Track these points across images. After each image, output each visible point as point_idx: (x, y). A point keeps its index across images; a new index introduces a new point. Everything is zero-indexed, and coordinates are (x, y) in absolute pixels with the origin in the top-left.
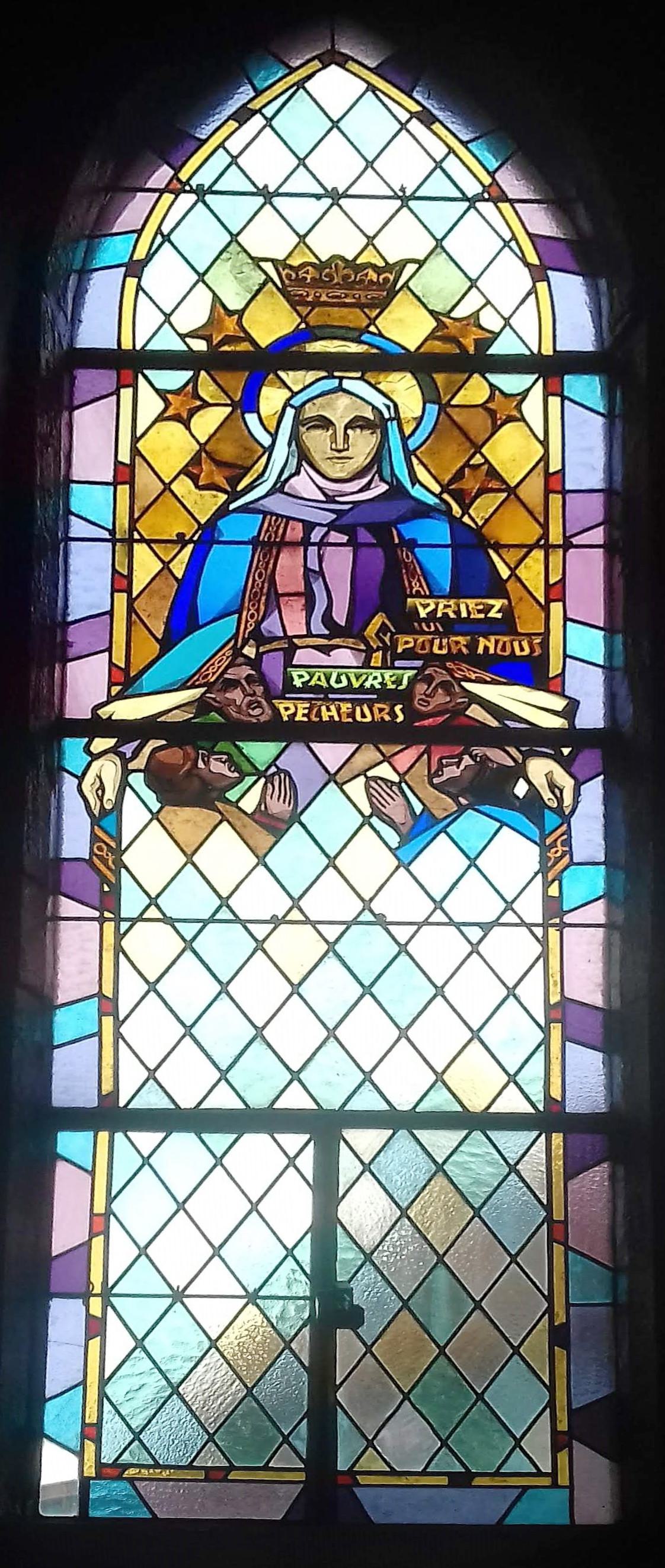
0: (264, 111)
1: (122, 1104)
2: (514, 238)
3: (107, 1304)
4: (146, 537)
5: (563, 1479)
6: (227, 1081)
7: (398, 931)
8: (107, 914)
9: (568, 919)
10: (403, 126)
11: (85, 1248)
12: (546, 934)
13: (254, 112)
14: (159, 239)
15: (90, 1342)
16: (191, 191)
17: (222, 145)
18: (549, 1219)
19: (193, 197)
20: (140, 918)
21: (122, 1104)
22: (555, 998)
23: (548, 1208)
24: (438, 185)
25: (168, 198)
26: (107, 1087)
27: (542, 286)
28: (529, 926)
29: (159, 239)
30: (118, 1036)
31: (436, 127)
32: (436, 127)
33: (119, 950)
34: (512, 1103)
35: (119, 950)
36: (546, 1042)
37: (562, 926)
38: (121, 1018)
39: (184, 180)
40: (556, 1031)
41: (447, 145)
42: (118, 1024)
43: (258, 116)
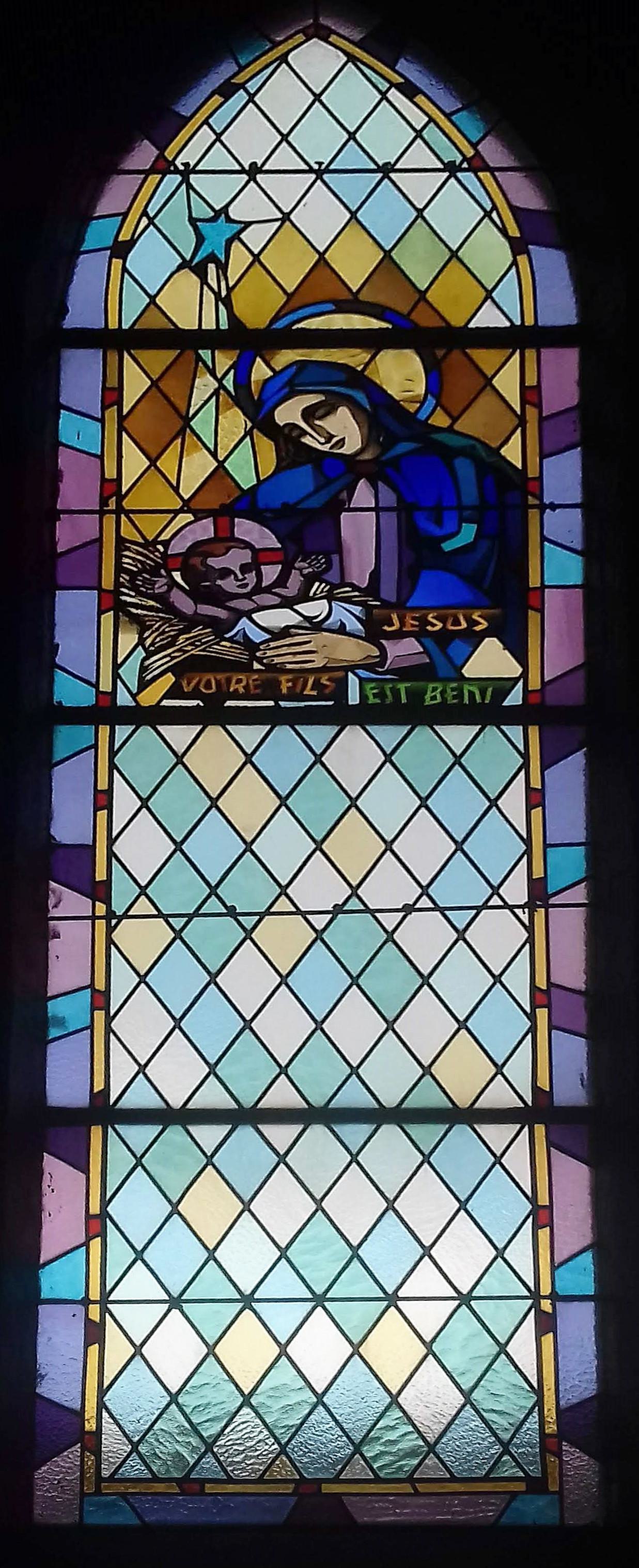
2: (495, 207)
3: (105, 1311)
5: (553, 1487)
7: (525, 918)
9: (552, 901)
14: (144, 221)
16: (177, 171)
17: (206, 122)
19: (179, 178)
22: (542, 983)
25: (154, 178)
26: (99, 1086)
27: (522, 260)
29: (144, 221)
30: (109, 1030)
31: (420, 99)
32: (420, 99)
33: (110, 942)
35: (110, 942)
36: (533, 1030)
37: (547, 907)
40: (542, 1014)
42: (109, 1019)
43: (242, 91)
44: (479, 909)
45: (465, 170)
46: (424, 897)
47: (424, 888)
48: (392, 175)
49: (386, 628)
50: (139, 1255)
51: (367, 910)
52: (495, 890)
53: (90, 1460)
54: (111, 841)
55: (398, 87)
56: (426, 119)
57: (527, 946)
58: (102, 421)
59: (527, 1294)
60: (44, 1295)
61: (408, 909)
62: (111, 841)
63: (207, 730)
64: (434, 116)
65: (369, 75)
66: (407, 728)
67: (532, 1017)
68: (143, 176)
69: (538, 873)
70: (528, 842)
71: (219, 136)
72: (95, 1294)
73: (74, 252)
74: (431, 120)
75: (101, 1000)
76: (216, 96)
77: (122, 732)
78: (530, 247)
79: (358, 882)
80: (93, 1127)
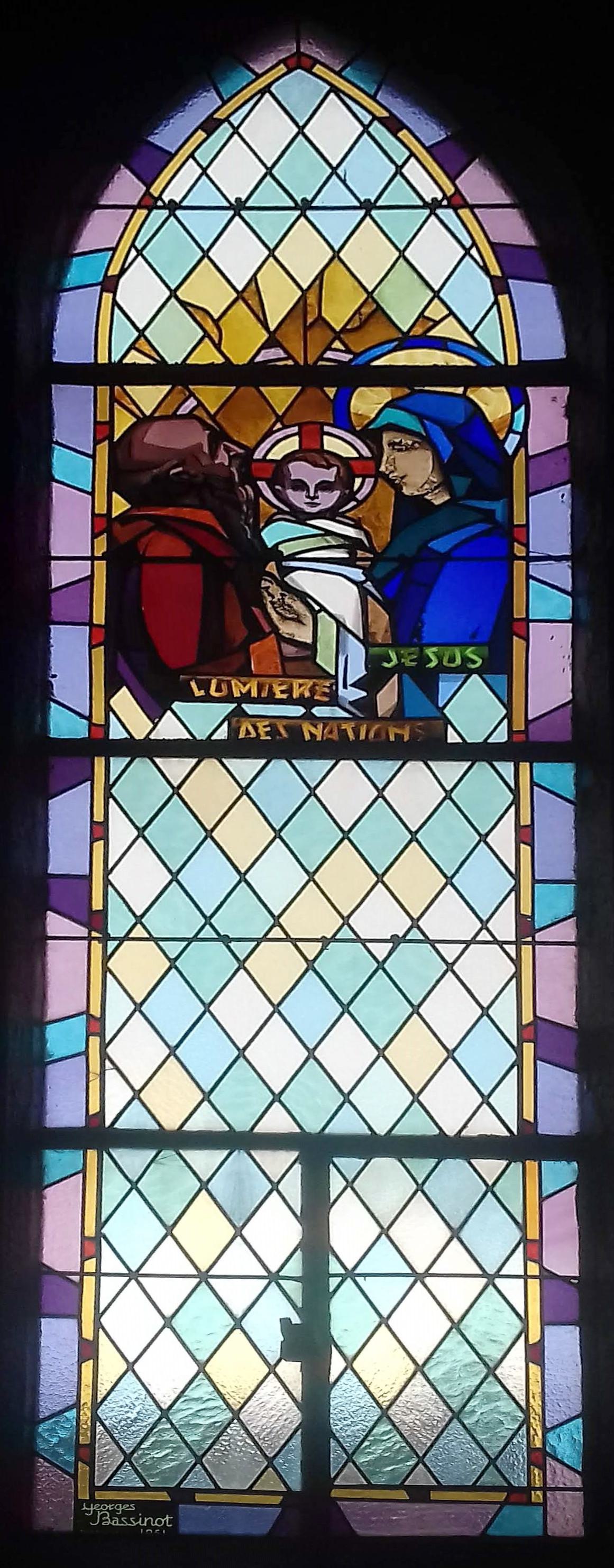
0: (231, 119)
1: (108, 1123)
2: (474, 244)
6: (210, 1102)
8: (94, 934)
10: (366, 129)
11: (99, 437)
13: (221, 122)
17: (192, 156)
18: (524, 1240)
19: (165, 213)
20: (126, 938)
21: (108, 1123)
22: (528, 1018)
23: (523, 1227)
24: (399, 193)
25: (141, 213)
26: (94, 1108)
27: (504, 299)
28: (501, 944)
29: (133, 253)
30: (104, 1056)
31: (403, 134)
32: (403, 134)
33: (106, 970)
34: (485, 1125)
36: (518, 1063)
39: (156, 195)
40: (529, 1048)
42: (104, 1046)
43: (226, 125)
44: (468, 943)
45: (445, 207)
48: (243, 213)
49: (386, 665)
51: (358, 939)
52: (484, 925)
55: (382, 121)
56: (407, 154)
57: (514, 981)
58: (93, 457)
61: (396, 941)
62: (107, 872)
63: (202, 764)
65: (355, 110)
66: (263, 762)
67: (519, 1051)
69: (526, 910)
70: (516, 876)
71: (204, 171)
73: (58, 289)
74: (412, 154)
75: (96, 1027)
77: (117, 764)
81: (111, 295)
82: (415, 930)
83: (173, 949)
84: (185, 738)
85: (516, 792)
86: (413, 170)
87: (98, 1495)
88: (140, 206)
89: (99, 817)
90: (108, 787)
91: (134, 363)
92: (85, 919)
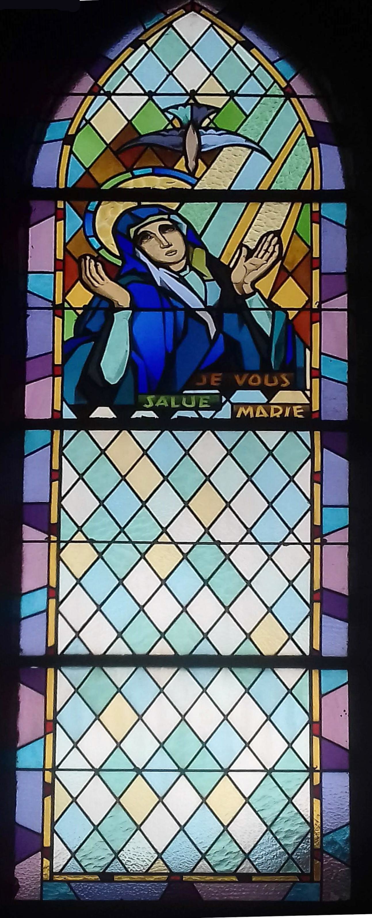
0: (147, 42)
1: (59, 652)
3: (54, 777)
4: (74, 306)
5: (317, 878)
10: (232, 49)
12: (312, 548)
14: (84, 122)
15: (46, 798)
17: (122, 64)
18: (311, 722)
21: (59, 652)
22: (317, 587)
23: (310, 714)
25: (90, 98)
26: (51, 643)
27: (315, 150)
29: (84, 122)
30: (58, 612)
31: (254, 51)
32: (254, 51)
33: (59, 559)
34: (290, 650)
35: (59, 559)
36: (311, 615)
38: (61, 599)
40: (317, 606)
41: (273, 78)
42: (59, 604)
43: (143, 46)
46: (249, 535)
47: (249, 532)
48: (236, 98)
50: (79, 581)
53: (46, 862)
54: (61, 498)
56: (257, 63)
59: (305, 769)
60: (29, 270)
64: (262, 62)
68: (83, 97)
69: (317, 523)
70: (311, 501)
72: (49, 765)
74: (260, 64)
75: (53, 593)
76: (130, 48)
77: (68, 434)
78: (321, 144)
79: (209, 525)
80: (48, 669)
81: (69, 147)
82: (249, 535)
83: (101, 547)
84: (112, 417)
85: (312, 450)
86: (260, 72)
87: (57, 878)
88: (90, 93)
89: (56, 467)
90: (62, 448)
91: (135, 188)
92: (46, 529)
